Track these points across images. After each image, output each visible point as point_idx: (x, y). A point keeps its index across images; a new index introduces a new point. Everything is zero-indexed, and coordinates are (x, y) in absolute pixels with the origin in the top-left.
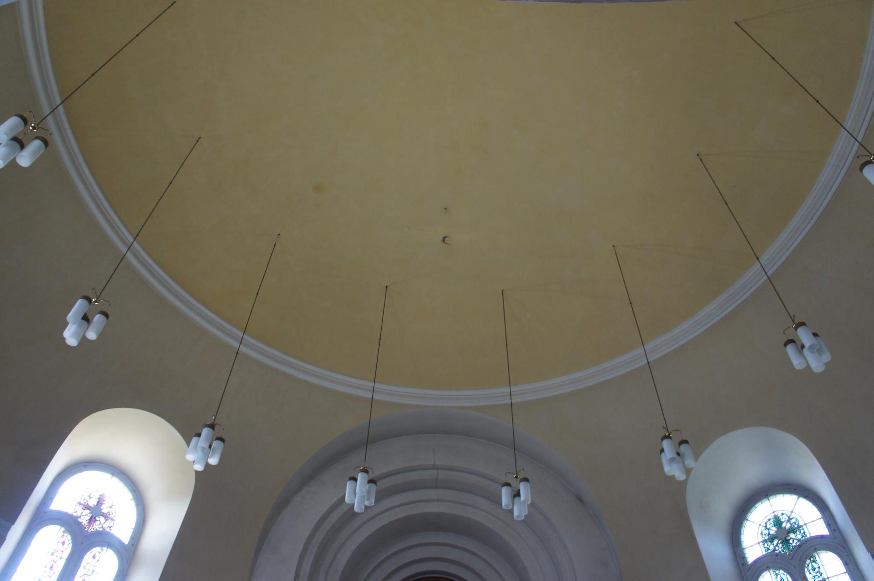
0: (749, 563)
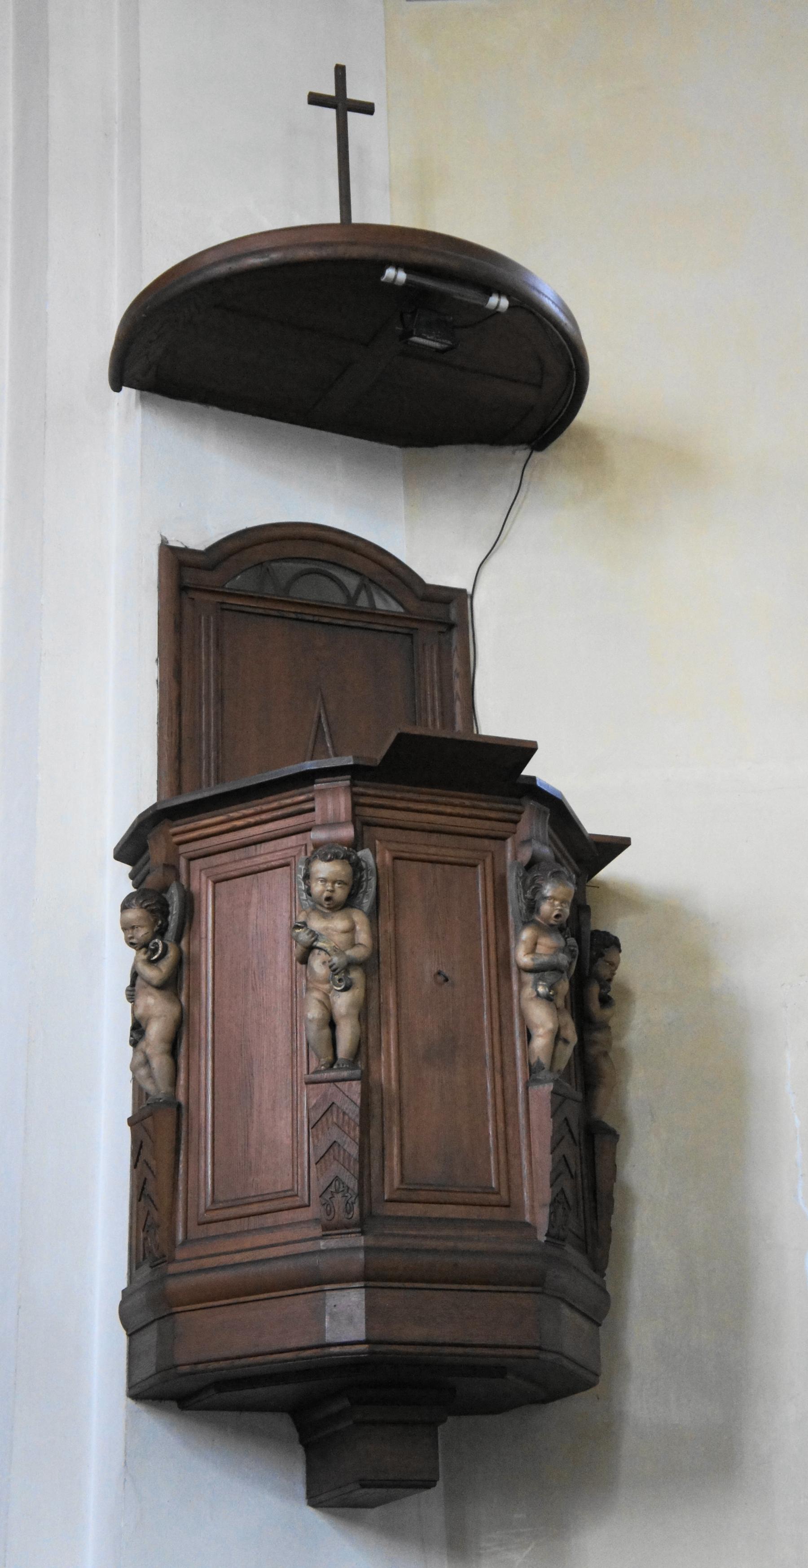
0: (356, 605)
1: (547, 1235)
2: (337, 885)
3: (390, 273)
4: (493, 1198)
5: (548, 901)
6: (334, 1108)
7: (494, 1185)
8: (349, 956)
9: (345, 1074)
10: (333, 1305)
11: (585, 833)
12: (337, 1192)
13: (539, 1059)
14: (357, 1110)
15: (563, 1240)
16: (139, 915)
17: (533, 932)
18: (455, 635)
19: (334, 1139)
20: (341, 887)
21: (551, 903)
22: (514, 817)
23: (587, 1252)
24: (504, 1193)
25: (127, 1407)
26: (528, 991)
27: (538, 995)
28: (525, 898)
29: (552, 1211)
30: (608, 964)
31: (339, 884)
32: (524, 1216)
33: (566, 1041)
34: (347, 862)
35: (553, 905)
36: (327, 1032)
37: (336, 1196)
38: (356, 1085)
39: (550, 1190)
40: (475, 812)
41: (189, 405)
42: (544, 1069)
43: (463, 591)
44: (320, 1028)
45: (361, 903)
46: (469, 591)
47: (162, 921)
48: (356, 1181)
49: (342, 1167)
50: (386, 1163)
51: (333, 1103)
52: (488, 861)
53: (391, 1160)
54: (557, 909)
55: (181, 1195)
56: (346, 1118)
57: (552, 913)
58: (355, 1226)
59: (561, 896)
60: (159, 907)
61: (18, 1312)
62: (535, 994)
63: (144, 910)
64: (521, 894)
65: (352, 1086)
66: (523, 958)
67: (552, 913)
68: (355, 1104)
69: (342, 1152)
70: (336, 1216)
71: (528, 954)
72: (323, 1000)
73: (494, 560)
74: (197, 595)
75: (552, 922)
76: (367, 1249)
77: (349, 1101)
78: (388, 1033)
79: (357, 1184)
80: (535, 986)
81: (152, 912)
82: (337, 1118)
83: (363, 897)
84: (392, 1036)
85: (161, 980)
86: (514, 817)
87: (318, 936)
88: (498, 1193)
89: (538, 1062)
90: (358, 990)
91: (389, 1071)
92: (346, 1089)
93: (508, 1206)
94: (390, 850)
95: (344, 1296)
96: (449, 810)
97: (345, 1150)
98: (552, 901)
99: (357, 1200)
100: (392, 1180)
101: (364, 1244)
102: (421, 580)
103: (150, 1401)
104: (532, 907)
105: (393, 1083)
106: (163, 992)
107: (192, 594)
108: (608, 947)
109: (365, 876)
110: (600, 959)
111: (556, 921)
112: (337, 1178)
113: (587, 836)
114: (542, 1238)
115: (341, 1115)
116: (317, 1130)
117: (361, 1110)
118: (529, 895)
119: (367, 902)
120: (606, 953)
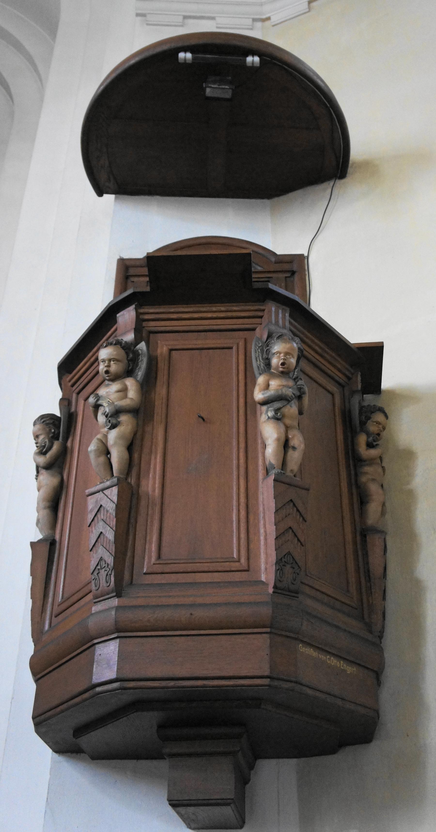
1: (274, 588)
2: (112, 362)
3: (182, 55)
4: (235, 566)
5: (275, 355)
6: (102, 509)
7: (235, 556)
8: (116, 405)
9: (108, 483)
10: (100, 654)
11: (349, 344)
12: (101, 569)
13: (270, 461)
14: (114, 506)
15: (297, 593)
16: (38, 427)
17: (264, 377)
18: (296, 277)
19: (101, 531)
20: (114, 363)
21: (278, 356)
22: (260, 314)
23: (363, 618)
24: (243, 560)
25: (52, 758)
26: (263, 418)
27: (269, 418)
28: (263, 359)
29: (277, 568)
30: (375, 423)
31: (113, 361)
32: (260, 577)
33: (294, 448)
34: (119, 346)
35: (279, 357)
36: (102, 459)
37: (101, 572)
38: (115, 489)
39: (275, 552)
40: (229, 314)
41: (142, 197)
42: (274, 468)
43: (302, 256)
44: (98, 456)
45: (137, 375)
46: (306, 254)
47: (54, 429)
48: (113, 558)
49: (105, 549)
50: (277, 594)
51: (101, 506)
52: (241, 344)
53: (151, 543)
54: (282, 359)
55: (50, 600)
56: (108, 514)
57: (279, 363)
58: (112, 592)
59: (285, 350)
60: (51, 421)
61: (11, 701)
62: (267, 417)
63: (42, 424)
64: (259, 356)
65: (112, 491)
66: (259, 396)
67: (279, 363)
68: (114, 502)
69: (105, 539)
70: (101, 586)
71: (260, 392)
72: (102, 438)
73: (320, 237)
74: (135, 279)
75: (281, 369)
76: (118, 608)
77: (110, 501)
78: (156, 458)
79: (113, 560)
80: (267, 411)
81: (47, 424)
82: (104, 515)
83: (138, 371)
84: (158, 460)
85: (45, 462)
86: (260, 314)
87: (100, 397)
88: (239, 561)
89: (270, 463)
90: (124, 427)
91: (154, 483)
92: (109, 494)
93: (248, 571)
94: (166, 345)
95: (107, 646)
96: (210, 315)
97: (107, 537)
98: (278, 355)
99: (113, 571)
100: (150, 558)
101: (118, 604)
102: (274, 254)
103: (69, 754)
104: (268, 365)
105: (157, 491)
106: (49, 471)
107: (132, 279)
108: (373, 412)
109: (141, 358)
110: (369, 421)
111: (283, 368)
112: (101, 559)
113: (353, 347)
114: (271, 590)
115: (105, 513)
116: (92, 528)
117: (116, 506)
118: (265, 356)
119: (140, 374)
120: (372, 416)
